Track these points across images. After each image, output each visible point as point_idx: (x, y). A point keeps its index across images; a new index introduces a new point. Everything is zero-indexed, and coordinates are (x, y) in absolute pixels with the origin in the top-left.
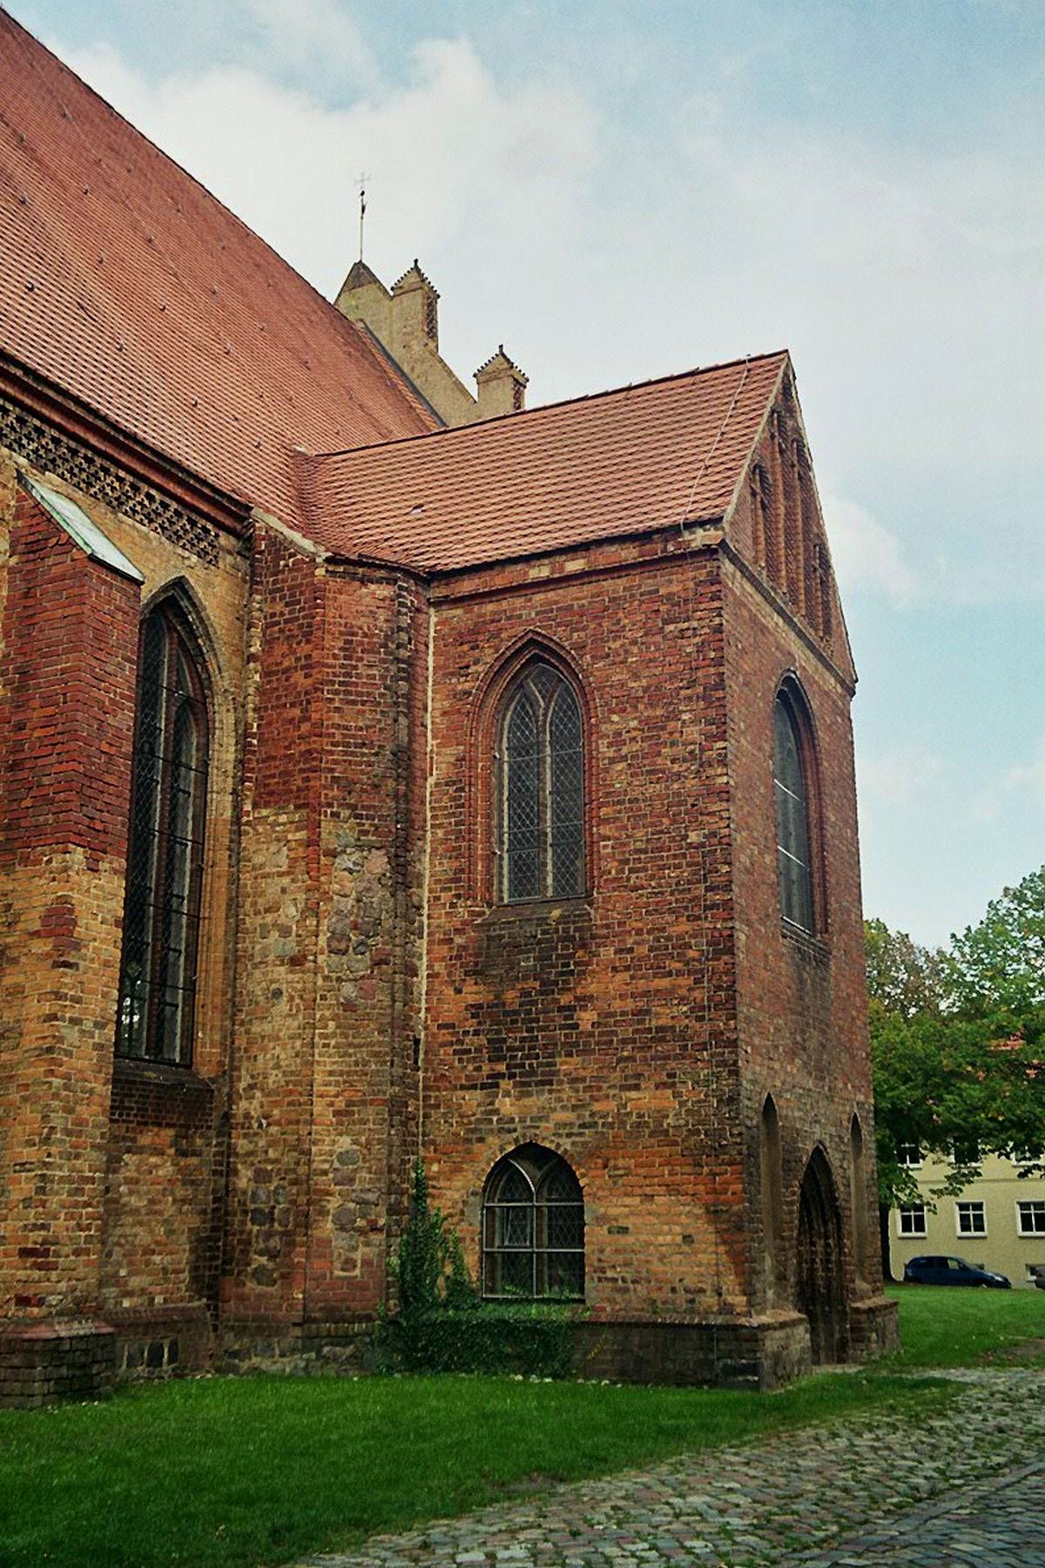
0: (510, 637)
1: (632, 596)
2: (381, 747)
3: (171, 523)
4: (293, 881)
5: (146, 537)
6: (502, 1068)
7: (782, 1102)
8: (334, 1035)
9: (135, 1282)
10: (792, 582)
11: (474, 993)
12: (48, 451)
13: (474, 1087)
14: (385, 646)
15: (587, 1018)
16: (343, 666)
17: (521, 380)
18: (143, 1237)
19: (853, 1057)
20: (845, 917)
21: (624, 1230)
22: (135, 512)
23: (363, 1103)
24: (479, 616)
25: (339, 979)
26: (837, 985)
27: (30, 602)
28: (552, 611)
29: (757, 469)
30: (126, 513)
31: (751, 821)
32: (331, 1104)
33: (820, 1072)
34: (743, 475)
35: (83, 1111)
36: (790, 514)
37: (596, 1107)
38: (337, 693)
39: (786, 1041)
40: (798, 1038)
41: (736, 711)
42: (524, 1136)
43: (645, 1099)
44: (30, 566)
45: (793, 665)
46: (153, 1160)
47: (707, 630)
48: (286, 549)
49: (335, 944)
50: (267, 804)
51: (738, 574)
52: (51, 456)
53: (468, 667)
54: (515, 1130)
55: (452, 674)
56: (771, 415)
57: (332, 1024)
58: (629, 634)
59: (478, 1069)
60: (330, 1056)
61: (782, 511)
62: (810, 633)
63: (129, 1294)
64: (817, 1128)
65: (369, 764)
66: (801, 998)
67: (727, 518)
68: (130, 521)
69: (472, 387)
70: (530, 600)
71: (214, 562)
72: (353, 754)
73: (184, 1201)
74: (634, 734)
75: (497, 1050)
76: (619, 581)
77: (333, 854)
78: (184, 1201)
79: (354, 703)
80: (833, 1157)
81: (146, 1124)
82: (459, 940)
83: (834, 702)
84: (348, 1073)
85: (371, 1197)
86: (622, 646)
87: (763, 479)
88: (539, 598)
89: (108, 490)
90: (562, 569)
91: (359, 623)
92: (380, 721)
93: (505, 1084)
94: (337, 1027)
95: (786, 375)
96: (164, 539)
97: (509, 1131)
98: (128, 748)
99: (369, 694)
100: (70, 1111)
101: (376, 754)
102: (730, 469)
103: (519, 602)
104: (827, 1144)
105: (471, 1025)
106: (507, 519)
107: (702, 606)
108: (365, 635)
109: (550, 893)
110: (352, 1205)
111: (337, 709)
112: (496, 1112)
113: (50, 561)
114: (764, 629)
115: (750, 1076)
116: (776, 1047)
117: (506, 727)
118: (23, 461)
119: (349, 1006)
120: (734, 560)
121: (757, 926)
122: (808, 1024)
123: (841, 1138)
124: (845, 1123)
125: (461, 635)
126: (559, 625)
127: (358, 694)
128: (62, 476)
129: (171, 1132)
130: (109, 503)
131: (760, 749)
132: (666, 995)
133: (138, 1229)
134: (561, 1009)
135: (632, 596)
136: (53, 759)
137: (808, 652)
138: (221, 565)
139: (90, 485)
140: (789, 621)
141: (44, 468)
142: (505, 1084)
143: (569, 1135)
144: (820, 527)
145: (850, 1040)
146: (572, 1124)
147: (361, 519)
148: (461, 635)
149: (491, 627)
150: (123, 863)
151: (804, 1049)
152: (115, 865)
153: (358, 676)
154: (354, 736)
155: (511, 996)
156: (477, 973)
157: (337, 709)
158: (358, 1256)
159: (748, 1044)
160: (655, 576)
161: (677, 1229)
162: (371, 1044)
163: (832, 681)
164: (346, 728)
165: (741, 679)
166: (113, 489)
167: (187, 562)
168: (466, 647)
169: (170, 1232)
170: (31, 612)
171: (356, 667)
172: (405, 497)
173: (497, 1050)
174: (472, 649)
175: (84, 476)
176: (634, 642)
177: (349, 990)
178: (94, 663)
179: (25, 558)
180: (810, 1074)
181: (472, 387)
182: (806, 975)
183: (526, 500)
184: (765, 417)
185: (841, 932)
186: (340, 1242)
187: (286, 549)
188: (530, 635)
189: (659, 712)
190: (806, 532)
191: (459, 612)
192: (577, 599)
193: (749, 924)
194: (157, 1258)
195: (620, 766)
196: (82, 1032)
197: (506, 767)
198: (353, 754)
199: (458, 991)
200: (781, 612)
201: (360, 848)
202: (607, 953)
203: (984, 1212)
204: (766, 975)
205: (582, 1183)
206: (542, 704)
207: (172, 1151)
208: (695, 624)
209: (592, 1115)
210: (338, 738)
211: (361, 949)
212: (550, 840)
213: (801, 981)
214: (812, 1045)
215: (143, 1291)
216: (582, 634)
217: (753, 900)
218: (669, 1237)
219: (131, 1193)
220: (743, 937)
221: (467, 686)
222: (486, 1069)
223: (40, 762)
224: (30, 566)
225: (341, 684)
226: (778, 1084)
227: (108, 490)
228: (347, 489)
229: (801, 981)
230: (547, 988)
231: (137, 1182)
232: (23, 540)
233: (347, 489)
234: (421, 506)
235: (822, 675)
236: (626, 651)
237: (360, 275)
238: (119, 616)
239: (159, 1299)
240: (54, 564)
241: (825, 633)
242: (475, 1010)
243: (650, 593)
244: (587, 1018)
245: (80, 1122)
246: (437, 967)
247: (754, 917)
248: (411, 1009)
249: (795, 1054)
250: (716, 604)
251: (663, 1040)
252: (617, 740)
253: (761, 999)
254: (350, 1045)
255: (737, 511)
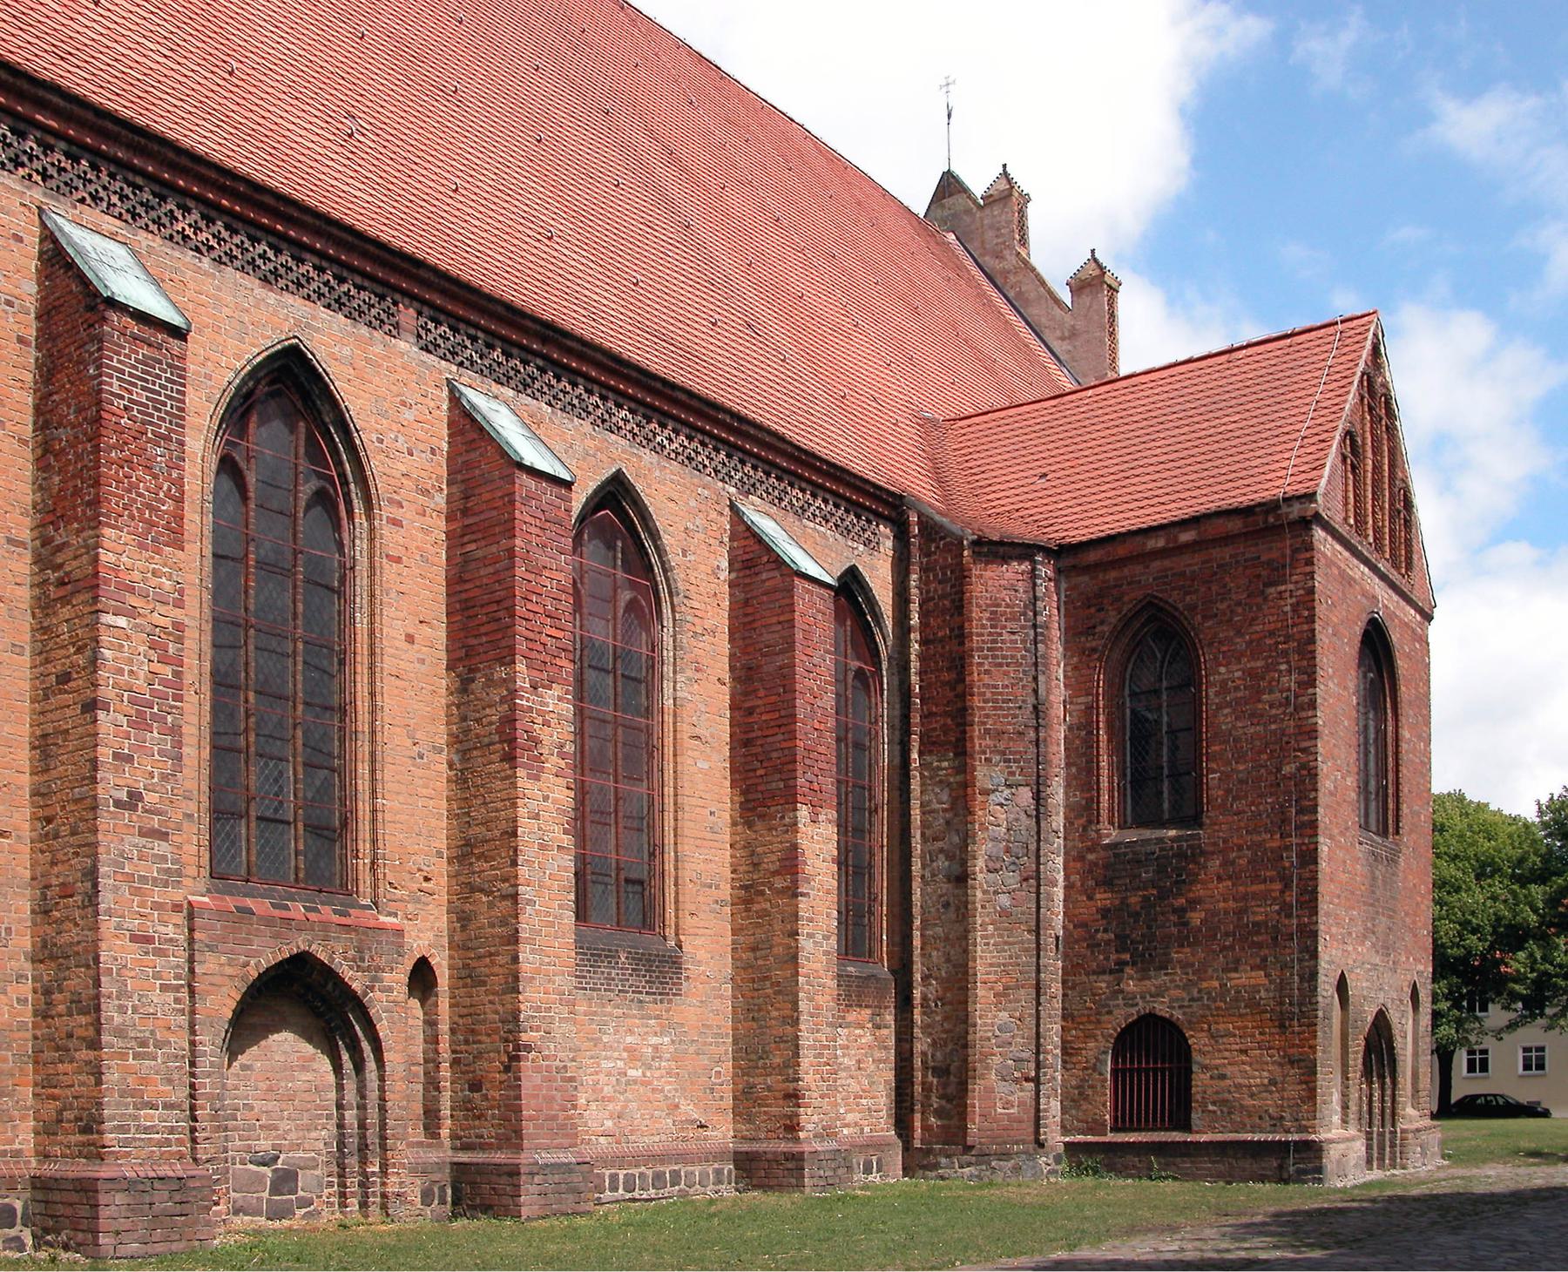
0: (1131, 601)
1: (1237, 562)
2: (1023, 701)
3: (842, 520)
4: (956, 815)
5: (824, 536)
6: (1127, 957)
7: (1353, 976)
8: (993, 935)
9: (850, 1117)
10: (1377, 531)
11: (1103, 898)
12: (749, 477)
13: (1104, 972)
14: (1025, 614)
15: (1196, 918)
16: (990, 634)
17: (1114, 285)
18: (854, 1087)
19: (1415, 936)
20: (1416, 819)
21: (1223, 1077)
22: (814, 515)
23: (1017, 987)
24: (1104, 582)
25: (996, 893)
26: (1406, 878)
27: (750, 610)
28: (1167, 576)
29: (1349, 434)
30: (808, 519)
31: (1336, 751)
32: (992, 988)
33: (1386, 949)
34: (1334, 447)
35: (820, 1000)
36: (1377, 468)
37: (1205, 985)
38: (986, 657)
39: (1358, 929)
40: (1369, 925)
41: (1325, 660)
42: (1144, 1008)
43: (1245, 978)
44: (747, 581)
45: (1377, 606)
46: (857, 1031)
47: (1301, 592)
48: (937, 533)
49: (991, 864)
50: (930, 752)
51: (1329, 538)
52: (752, 481)
53: (1094, 627)
54: (1137, 1004)
55: (1081, 633)
56: (1361, 381)
57: (991, 927)
58: (1234, 597)
59: (1107, 959)
60: (990, 952)
61: (1369, 468)
62: (1394, 575)
63: (847, 1126)
64: (1381, 995)
65: (1015, 716)
66: (1373, 892)
67: (1320, 491)
68: (812, 525)
69: (1066, 297)
70: (1148, 567)
71: (876, 549)
72: (1001, 708)
73: (880, 1061)
74: (1238, 682)
75: (1122, 942)
76: (1226, 549)
77: (986, 792)
78: (880, 1061)
79: (1001, 665)
80: (1393, 1017)
81: (851, 1006)
82: (1091, 857)
83: (1413, 631)
84: (1004, 965)
85: (1025, 1055)
86: (1229, 606)
87: (1353, 442)
88: (1156, 565)
89: (794, 501)
90: (1176, 539)
91: (1002, 595)
92: (1021, 679)
93: (1129, 970)
94: (995, 929)
95: (1375, 335)
96: (837, 535)
97: (1132, 1006)
98: (831, 723)
99: (1012, 657)
100: (811, 1000)
101: (1020, 708)
102: (1323, 441)
103: (1138, 569)
104: (1389, 1006)
105: (1102, 924)
106: (1125, 490)
107: (1298, 571)
108: (1008, 606)
109: (1166, 816)
110: (1010, 1062)
111: (987, 672)
112: (1122, 991)
113: (764, 576)
114: (1351, 581)
115: (1327, 958)
116: (1350, 934)
117: (1128, 677)
118: (733, 490)
119: (1004, 913)
120: (1327, 527)
121: (1338, 838)
122: (1377, 913)
123: (1401, 1001)
124: (1405, 989)
125: (1088, 599)
126: (1173, 589)
127: (1004, 657)
128: (761, 497)
129: (869, 1011)
130: (796, 513)
131: (1345, 688)
132: (1263, 896)
133: (850, 1081)
134: (1175, 911)
135: (1237, 562)
136: (780, 737)
137: (1390, 592)
138: (882, 550)
139: (781, 500)
140: (1374, 568)
141: (748, 492)
142: (1129, 970)
143: (1180, 1007)
144: (1404, 471)
145: (1414, 922)
146: (1183, 999)
147: (993, 489)
148: (1088, 599)
149: (1115, 592)
150: (833, 814)
151: (1374, 933)
152: (830, 817)
153: (1003, 642)
154: (1001, 694)
155: (1134, 900)
156: (1107, 883)
157: (987, 672)
158: (1014, 1098)
159: (1327, 933)
160: (1257, 545)
161: (1266, 1074)
162: (1022, 942)
163: (1412, 612)
164: (995, 687)
165: (1330, 631)
166: (798, 499)
167: (856, 552)
168: (1093, 610)
169: (871, 1084)
170: (750, 618)
171: (1001, 634)
172: (1030, 466)
173: (1122, 942)
174: (1099, 611)
175: (776, 493)
176: (1239, 604)
177: (1004, 900)
178: (805, 658)
179: (741, 575)
180: (1377, 952)
181: (1066, 297)
182: (1377, 873)
183: (1141, 470)
184: (1356, 383)
185: (1411, 831)
186: (1002, 1088)
187: (937, 533)
188: (1148, 599)
189: (1259, 664)
190: (1392, 477)
191: (1086, 578)
192: (1190, 565)
193: (1331, 837)
194: (864, 1101)
195: (1226, 711)
196: (815, 942)
197: (1128, 711)
198: (1001, 708)
199: (1090, 898)
200: (1366, 562)
201: (1010, 786)
202: (1215, 864)
203: (1490, 1056)
204: (1344, 877)
205: (1190, 1042)
206: (1159, 655)
207: (870, 1025)
208: (1291, 587)
209: (1200, 991)
210: (988, 695)
211: (1012, 868)
212: (1166, 771)
213: (1374, 878)
214: (1380, 929)
215: (856, 1124)
216: (1194, 597)
217: (1336, 817)
218: (1259, 1078)
219: (844, 1056)
220: (1326, 849)
221: (1094, 644)
222: (1113, 957)
223: (770, 740)
224: (747, 581)
225: (989, 649)
226: (1351, 962)
227: (794, 501)
228: (975, 456)
229: (1374, 878)
230: (1163, 895)
231: (848, 1047)
232: (739, 559)
233: (975, 456)
234: (1045, 475)
235: (1403, 609)
236: (1232, 611)
237: (949, 185)
238: (820, 616)
239: (867, 1129)
240: (769, 577)
241: (1407, 570)
242: (1105, 913)
243: (1253, 559)
244: (1196, 918)
245: (817, 1008)
246: (1073, 878)
247: (1336, 831)
248: (1052, 913)
249: (1365, 937)
250: (1308, 569)
251: (1258, 933)
252: (1224, 688)
253: (1339, 897)
254: (1006, 943)
255: (1329, 482)
